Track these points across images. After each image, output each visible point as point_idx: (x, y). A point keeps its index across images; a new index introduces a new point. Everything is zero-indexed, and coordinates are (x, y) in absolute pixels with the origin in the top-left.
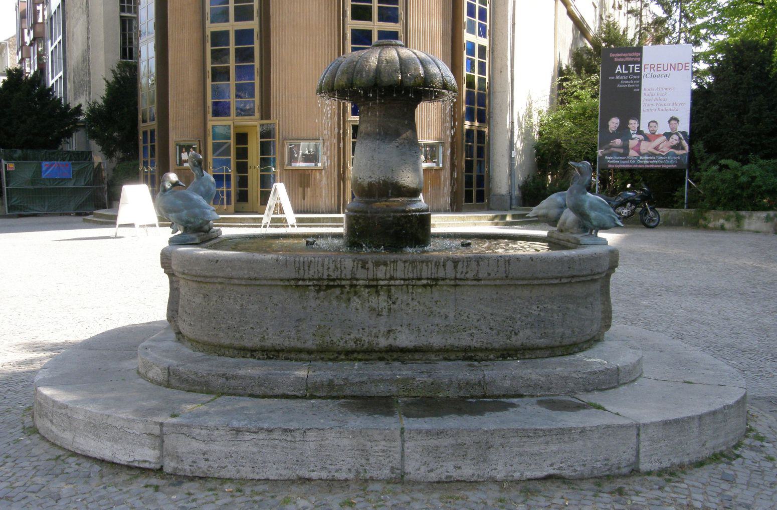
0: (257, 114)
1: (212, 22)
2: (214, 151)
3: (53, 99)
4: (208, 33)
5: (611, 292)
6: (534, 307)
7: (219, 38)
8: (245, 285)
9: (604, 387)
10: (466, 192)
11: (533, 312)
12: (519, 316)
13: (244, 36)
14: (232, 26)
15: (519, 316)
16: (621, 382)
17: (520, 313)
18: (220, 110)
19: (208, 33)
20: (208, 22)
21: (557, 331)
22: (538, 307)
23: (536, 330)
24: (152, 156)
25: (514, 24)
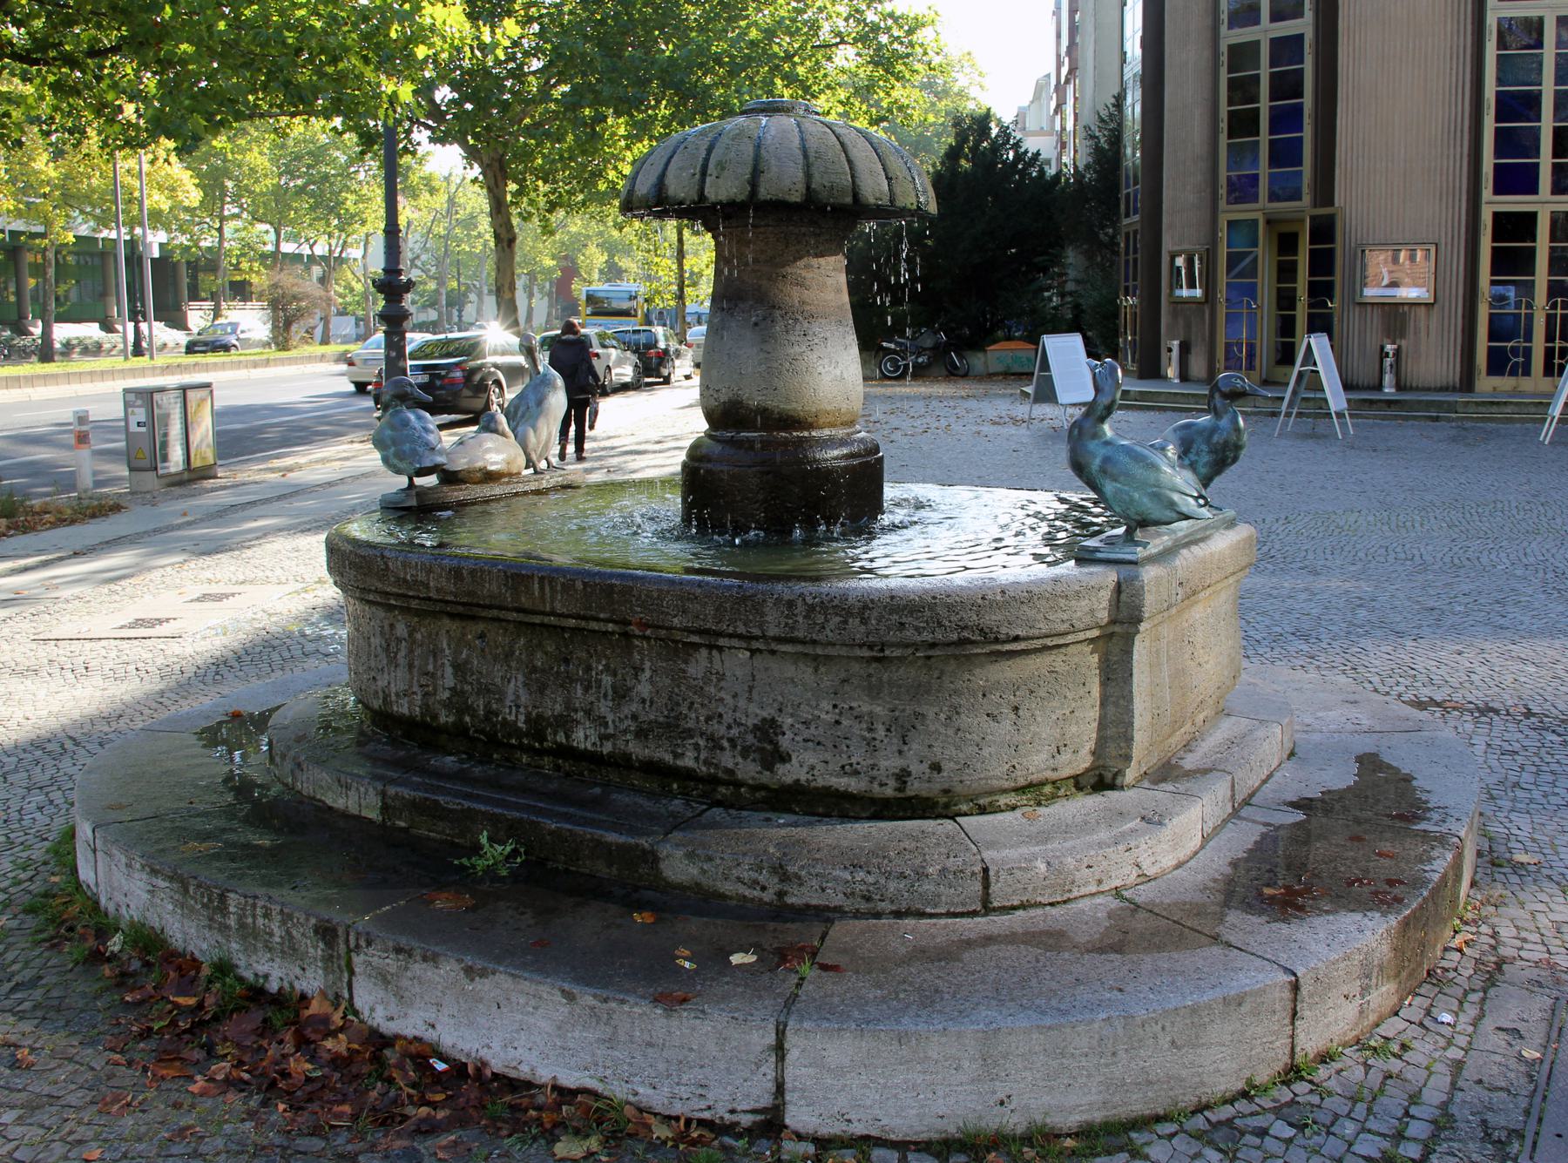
0: (1307, 198)
1: (1230, 27)
2: (1230, 268)
3: (1019, 183)
4: (1224, 49)
5: (1135, 657)
6: (826, 705)
7: (1242, 55)
8: (478, 605)
9: (928, 910)
10: (1547, 349)
11: (823, 716)
12: (790, 721)
13: (1287, 48)
14: (1265, 31)
15: (790, 721)
16: (996, 904)
17: (792, 715)
18: (1243, 190)
19: (1224, 49)
20: (1224, 29)
21: (883, 764)
22: (835, 706)
23: (828, 756)
24: (1135, 279)
25: (1059, 36)
